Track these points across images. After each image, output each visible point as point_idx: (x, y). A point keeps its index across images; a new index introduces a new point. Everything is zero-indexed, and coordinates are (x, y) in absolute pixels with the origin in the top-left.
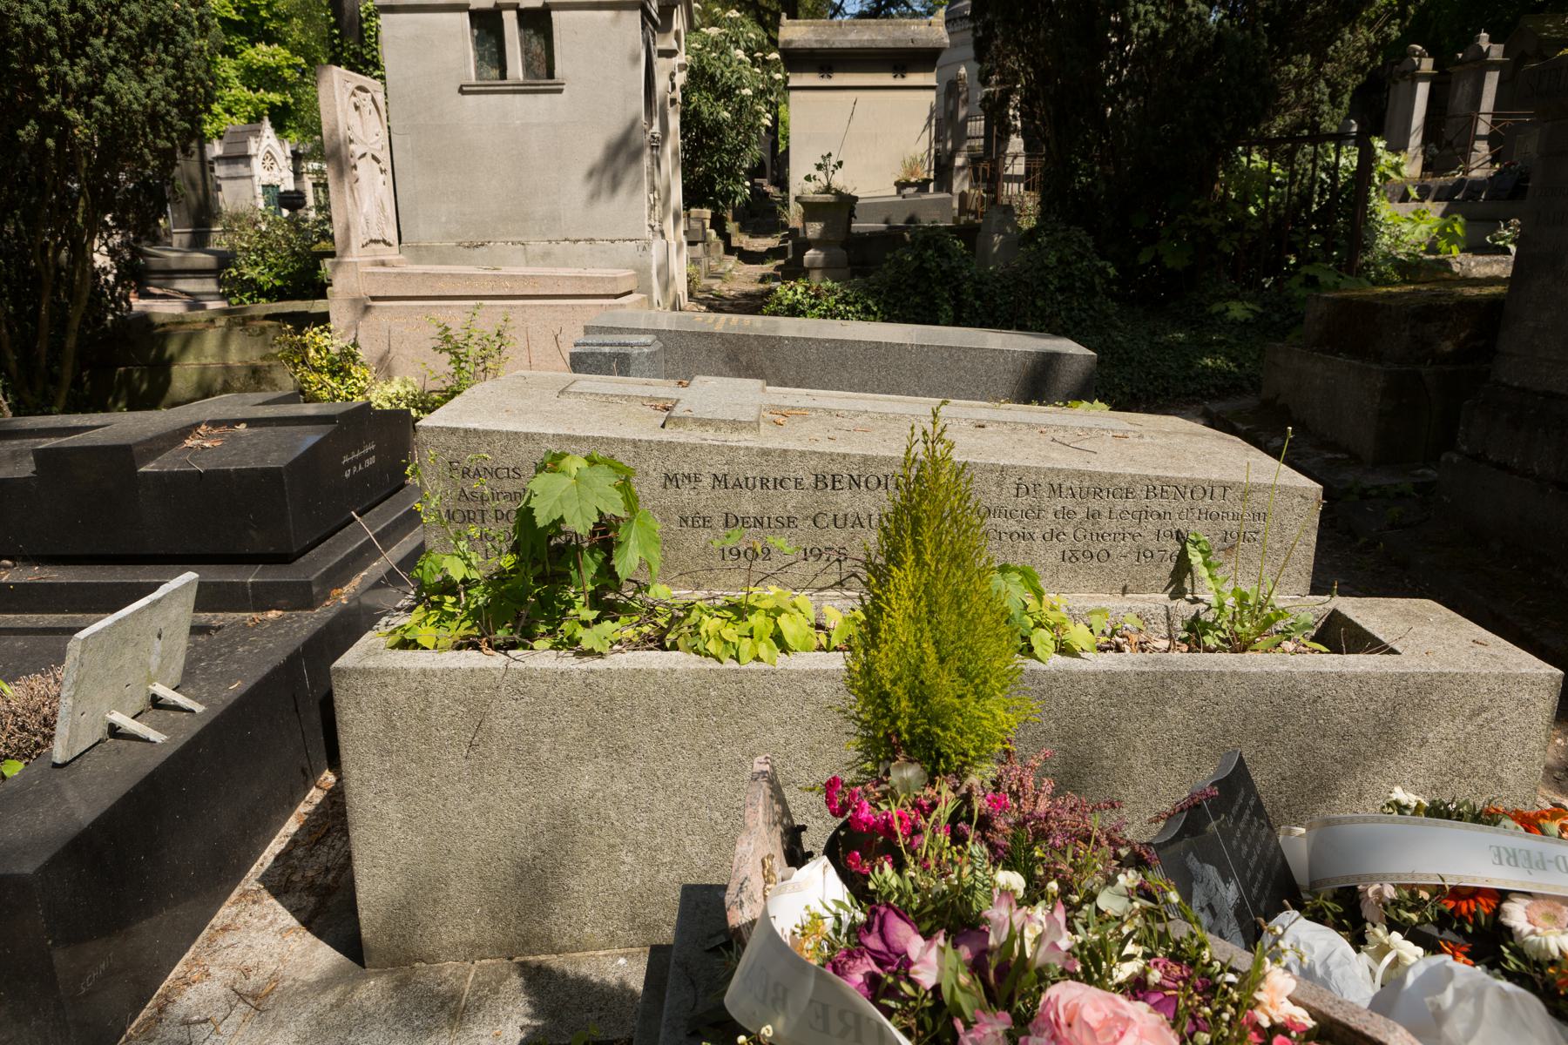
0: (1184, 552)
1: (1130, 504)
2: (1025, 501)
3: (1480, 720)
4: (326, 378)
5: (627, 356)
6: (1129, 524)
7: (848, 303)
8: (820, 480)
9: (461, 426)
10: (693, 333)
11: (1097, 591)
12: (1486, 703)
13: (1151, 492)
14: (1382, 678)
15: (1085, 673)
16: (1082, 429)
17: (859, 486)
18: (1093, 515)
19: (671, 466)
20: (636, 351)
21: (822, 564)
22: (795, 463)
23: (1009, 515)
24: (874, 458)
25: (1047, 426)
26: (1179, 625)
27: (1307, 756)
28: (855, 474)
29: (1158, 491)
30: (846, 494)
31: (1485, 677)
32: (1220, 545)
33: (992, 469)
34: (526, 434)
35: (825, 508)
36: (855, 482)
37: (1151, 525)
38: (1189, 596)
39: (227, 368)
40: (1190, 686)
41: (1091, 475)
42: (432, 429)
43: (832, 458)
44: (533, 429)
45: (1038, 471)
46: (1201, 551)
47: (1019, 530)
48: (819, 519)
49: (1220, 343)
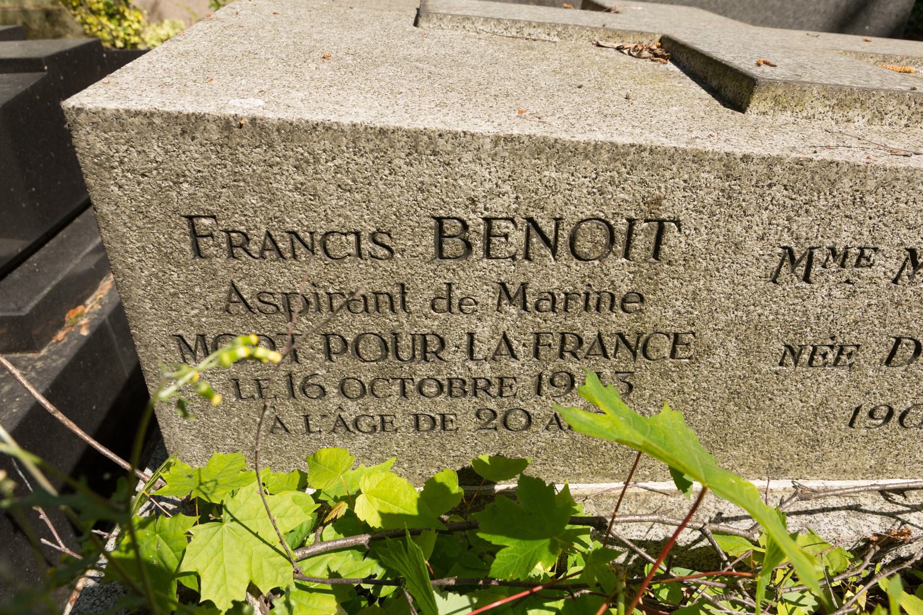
4: (104, 20)
9: (209, 108)
19: (805, 230)
34: (414, 136)
39: (25, 12)
42: (120, 120)
44: (429, 120)
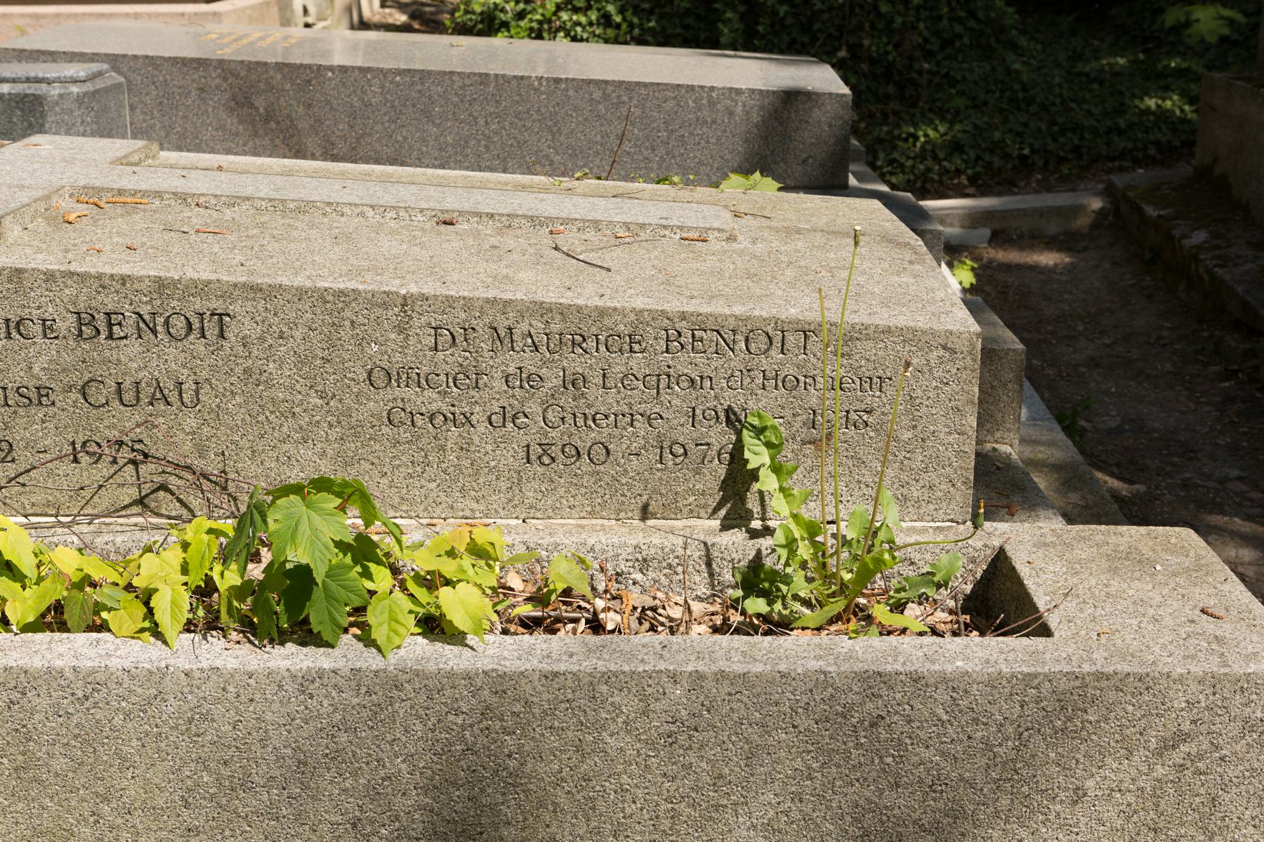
0: (739, 446)
1: (637, 363)
2: (449, 359)
3: (1177, 757)
5: (38, 100)
6: (639, 397)
7: (576, 10)
8: (84, 320)
10: (174, 61)
11: (592, 514)
12: (1186, 726)
13: (673, 340)
14: (993, 683)
15: (451, 675)
16: (626, 225)
17: (154, 332)
18: (574, 382)
20: (55, 91)
21: (105, 469)
22: (40, 295)
23: (425, 382)
24: (175, 283)
25: (566, 221)
26: (728, 577)
27: (869, 820)
28: (145, 310)
29: (687, 338)
30: (133, 347)
31: (1180, 680)
32: (804, 433)
33: (384, 300)
35: (99, 371)
36: (146, 326)
37: (679, 397)
38: (756, 524)
40: (644, 698)
41: (563, 311)
43: (102, 282)
45: (468, 304)
46: (768, 445)
47: (445, 409)
48: (91, 390)
49: (1180, 73)
